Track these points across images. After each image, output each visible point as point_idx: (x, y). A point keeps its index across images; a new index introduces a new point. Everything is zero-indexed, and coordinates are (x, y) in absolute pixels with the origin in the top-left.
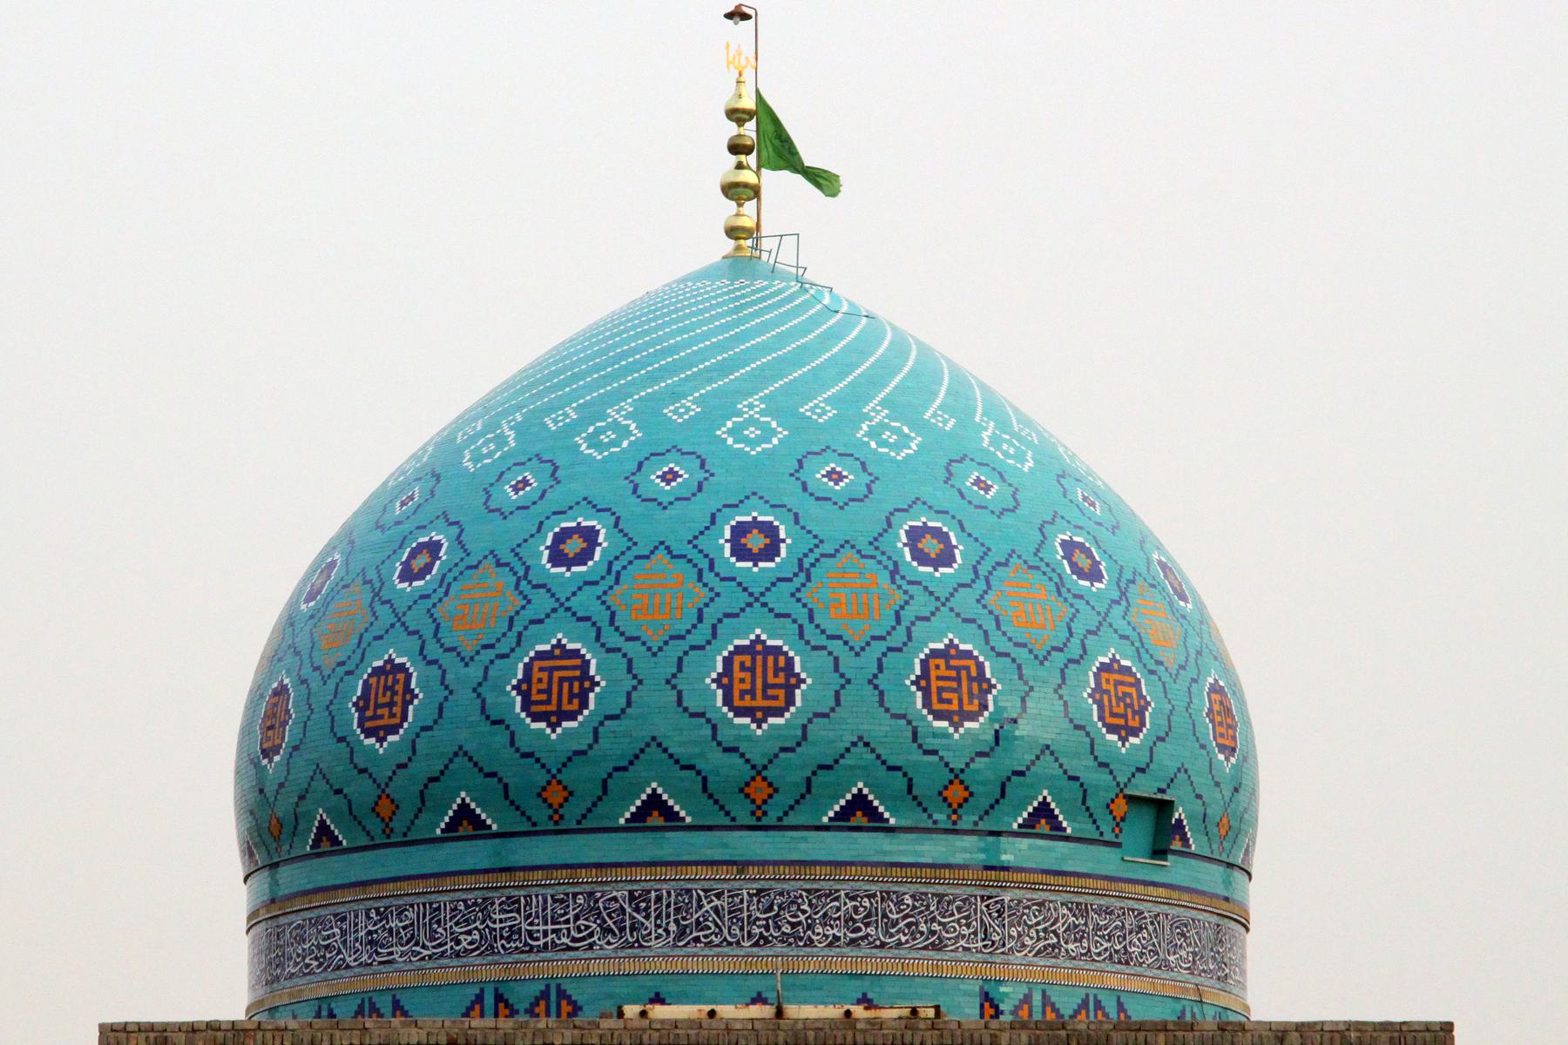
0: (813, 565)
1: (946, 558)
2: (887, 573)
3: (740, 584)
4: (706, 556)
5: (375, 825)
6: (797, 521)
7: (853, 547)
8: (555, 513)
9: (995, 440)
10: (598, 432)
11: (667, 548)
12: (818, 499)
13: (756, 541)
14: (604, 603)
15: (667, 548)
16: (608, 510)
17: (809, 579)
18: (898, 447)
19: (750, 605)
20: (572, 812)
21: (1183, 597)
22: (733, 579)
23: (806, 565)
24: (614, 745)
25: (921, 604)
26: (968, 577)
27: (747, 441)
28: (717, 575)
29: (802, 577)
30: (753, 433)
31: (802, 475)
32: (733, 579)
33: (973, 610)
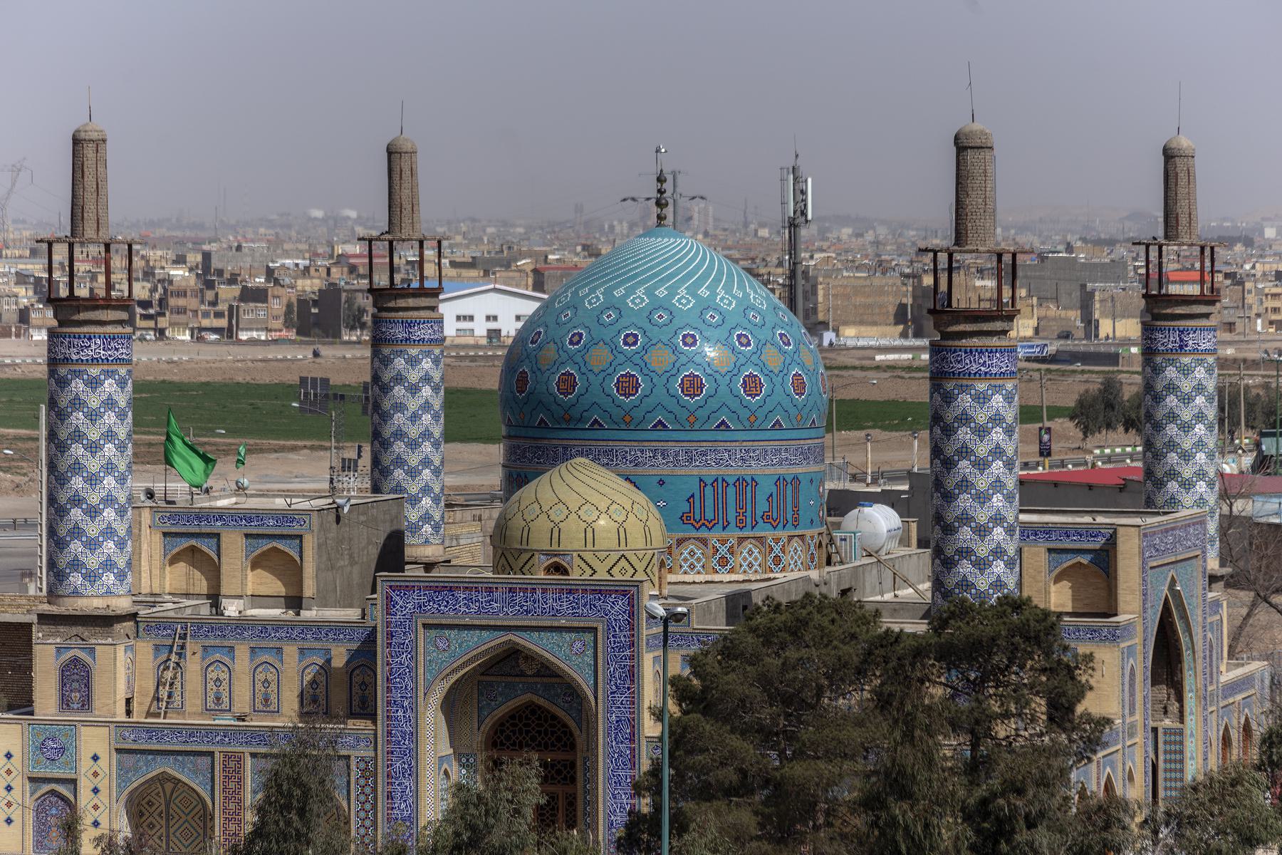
20: (756, 424)
24: (714, 405)
33: (639, 361)
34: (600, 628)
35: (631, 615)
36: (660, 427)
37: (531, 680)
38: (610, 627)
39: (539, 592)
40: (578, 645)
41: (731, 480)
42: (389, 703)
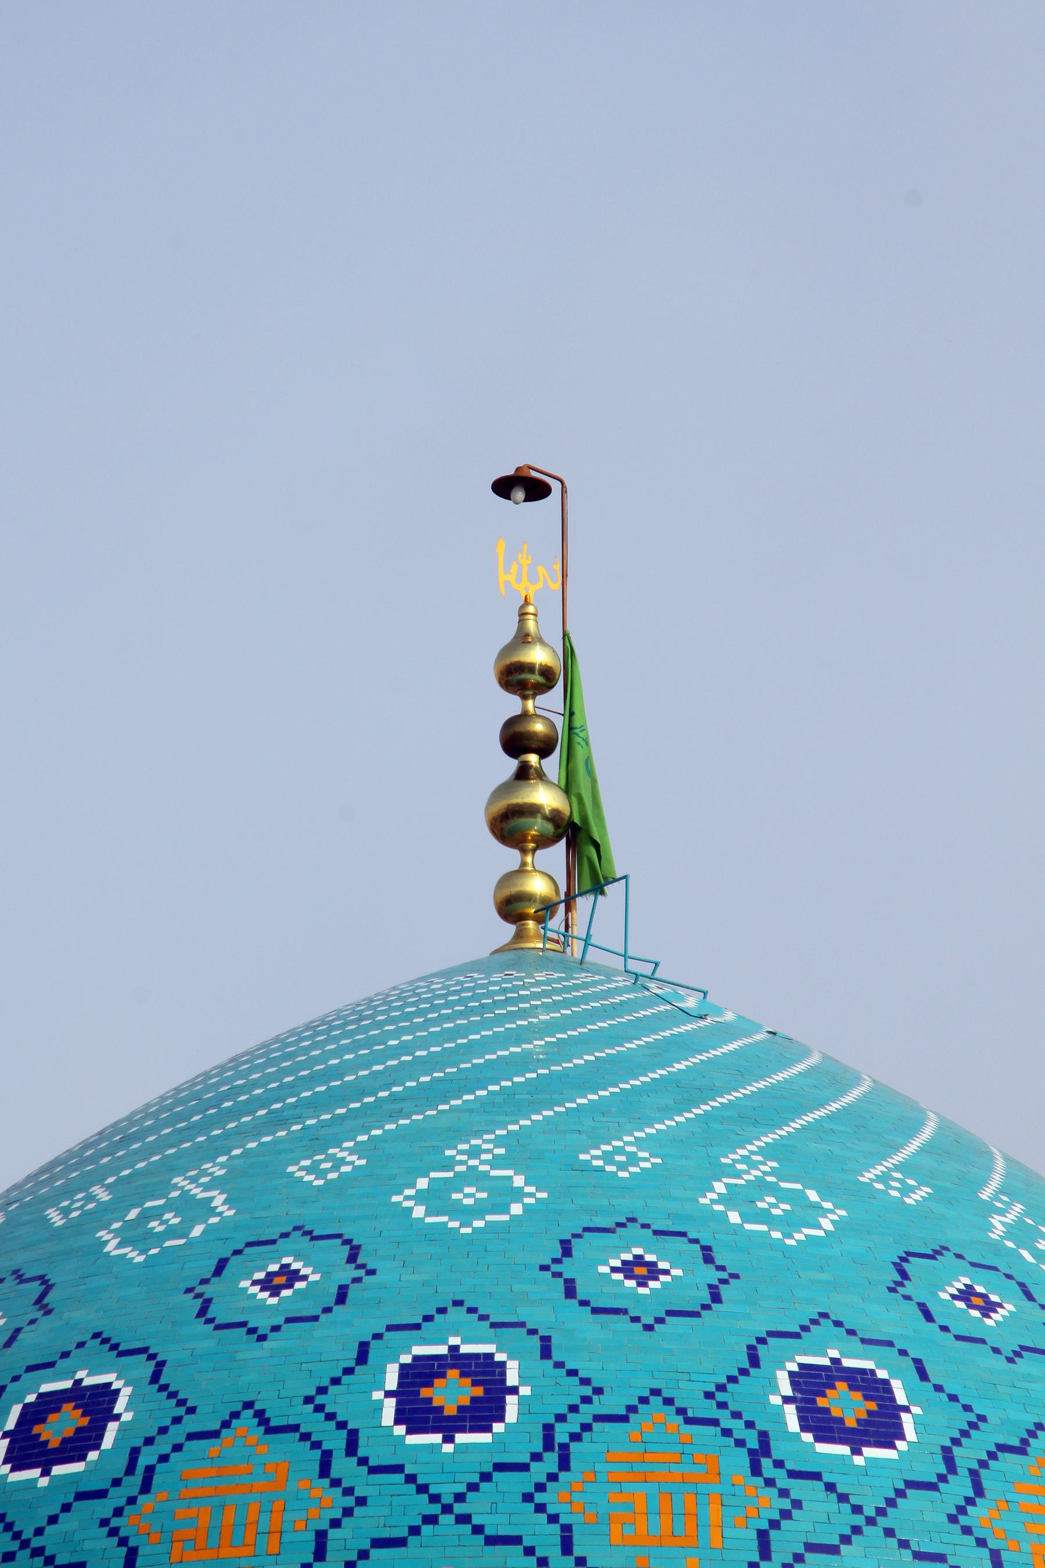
0: (575, 1437)
1: (882, 1426)
2: (743, 1459)
3: (411, 1479)
4: (342, 1425)
6: (546, 1352)
7: (669, 1402)
8: (30, 1369)
11: (260, 1414)
12: (596, 1311)
13: (451, 1393)
14: (113, 1532)
15: (260, 1414)
16: (144, 1350)
17: (564, 1464)
18: (789, 1223)
19: (431, 1520)
22: (398, 1469)
23: (561, 1435)
25: (818, 1516)
26: (931, 1468)
28: (363, 1461)
29: (551, 1461)
30: (472, 1197)
32: (398, 1469)
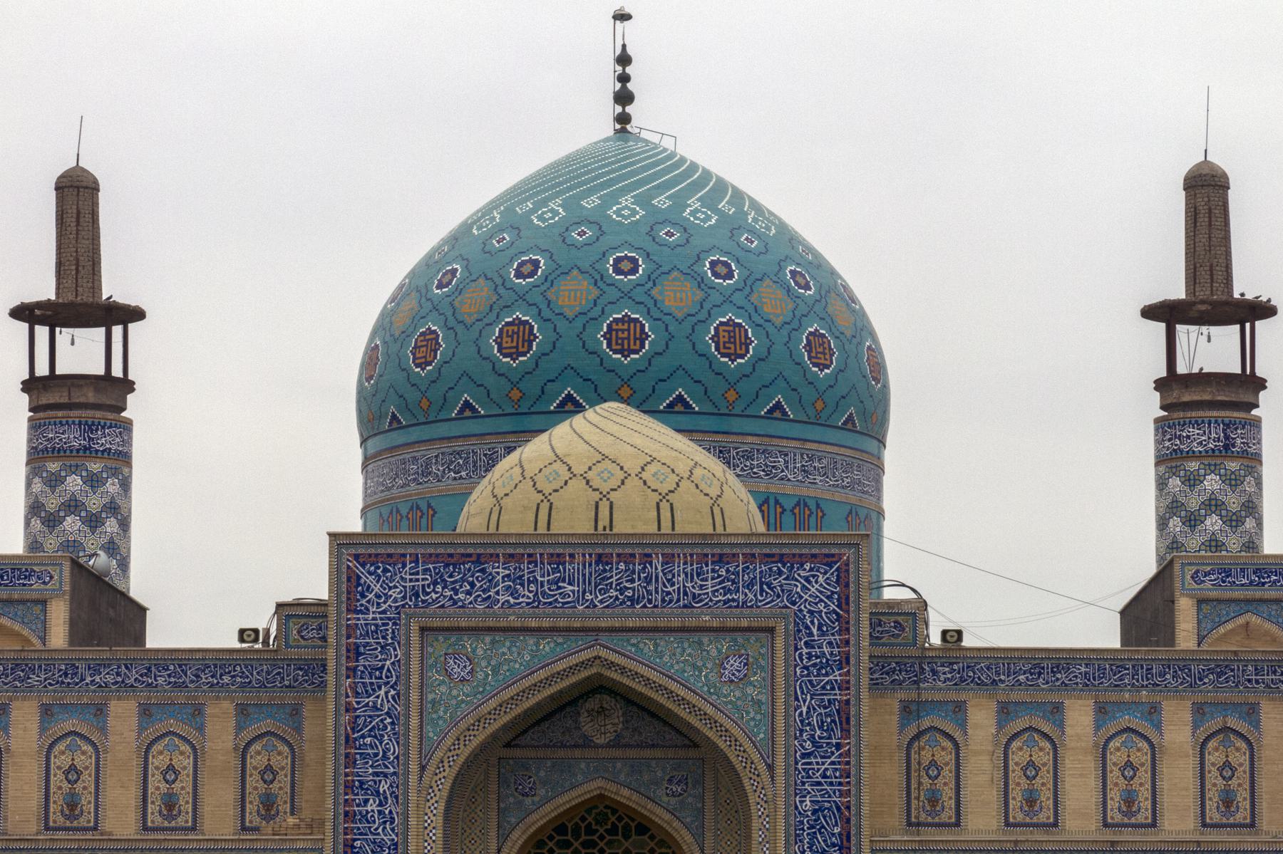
1: (730, 275)
5: (811, 412)
9: (755, 220)
10: (544, 213)
21: (854, 302)
27: (623, 216)
31: (686, 235)
33: (643, 298)
34: (780, 629)
35: (844, 602)
36: (679, 408)
37: (603, 753)
38: (800, 627)
39: (658, 562)
40: (734, 664)
41: (788, 504)
42: (349, 787)
